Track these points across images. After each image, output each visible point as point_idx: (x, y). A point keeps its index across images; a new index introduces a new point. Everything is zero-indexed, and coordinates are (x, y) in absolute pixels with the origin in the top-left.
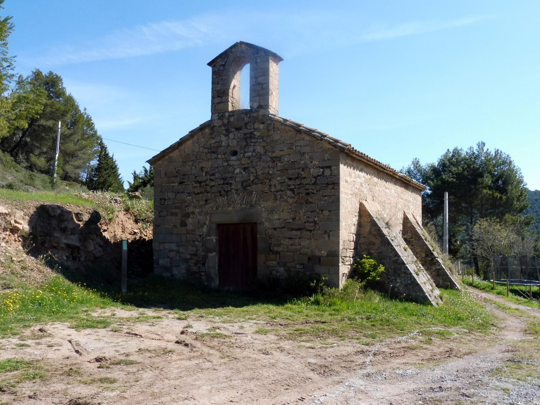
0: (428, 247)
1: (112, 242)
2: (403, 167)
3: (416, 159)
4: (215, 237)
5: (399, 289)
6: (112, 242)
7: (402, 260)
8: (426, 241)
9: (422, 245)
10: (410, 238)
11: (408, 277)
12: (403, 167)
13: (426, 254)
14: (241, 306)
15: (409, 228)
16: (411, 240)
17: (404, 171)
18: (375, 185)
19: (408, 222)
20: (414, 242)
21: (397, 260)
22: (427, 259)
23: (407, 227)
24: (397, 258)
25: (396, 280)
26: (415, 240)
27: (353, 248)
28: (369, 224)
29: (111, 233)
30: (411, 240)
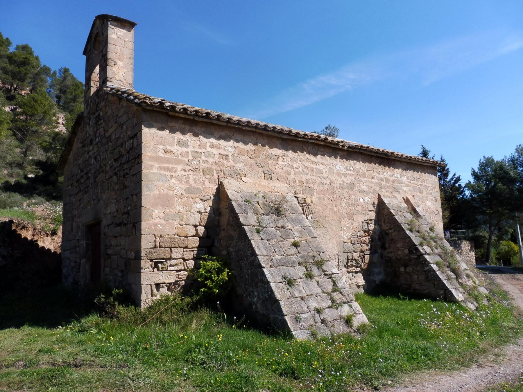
0: (411, 241)
1: (52, 251)
2: (505, 157)
3: (520, 145)
4: (85, 242)
5: (257, 307)
6: (52, 251)
7: (259, 261)
8: (411, 231)
9: (403, 237)
10: (388, 229)
11: (266, 288)
12: (505, 157)
13: (409, 250)
14: (52, 324)
15: (386, 215)
16: (390, 231)
17: (507, 160)
18: (355, 164)
19: (384, 208)
20: (393, 234)
21: (254, 261)
22: (412, 256)
23: (383, 214)
24: (253, 257)
25: (253, 292)
26: (395, 231)
27: (197, 245)
28: (228, 210)
29: (57, 243)
30: (390, 231)
